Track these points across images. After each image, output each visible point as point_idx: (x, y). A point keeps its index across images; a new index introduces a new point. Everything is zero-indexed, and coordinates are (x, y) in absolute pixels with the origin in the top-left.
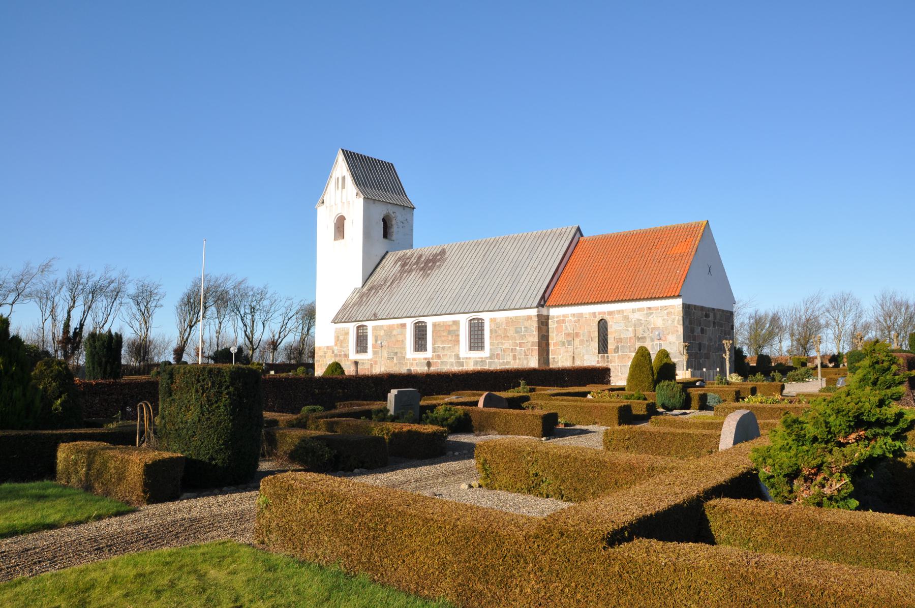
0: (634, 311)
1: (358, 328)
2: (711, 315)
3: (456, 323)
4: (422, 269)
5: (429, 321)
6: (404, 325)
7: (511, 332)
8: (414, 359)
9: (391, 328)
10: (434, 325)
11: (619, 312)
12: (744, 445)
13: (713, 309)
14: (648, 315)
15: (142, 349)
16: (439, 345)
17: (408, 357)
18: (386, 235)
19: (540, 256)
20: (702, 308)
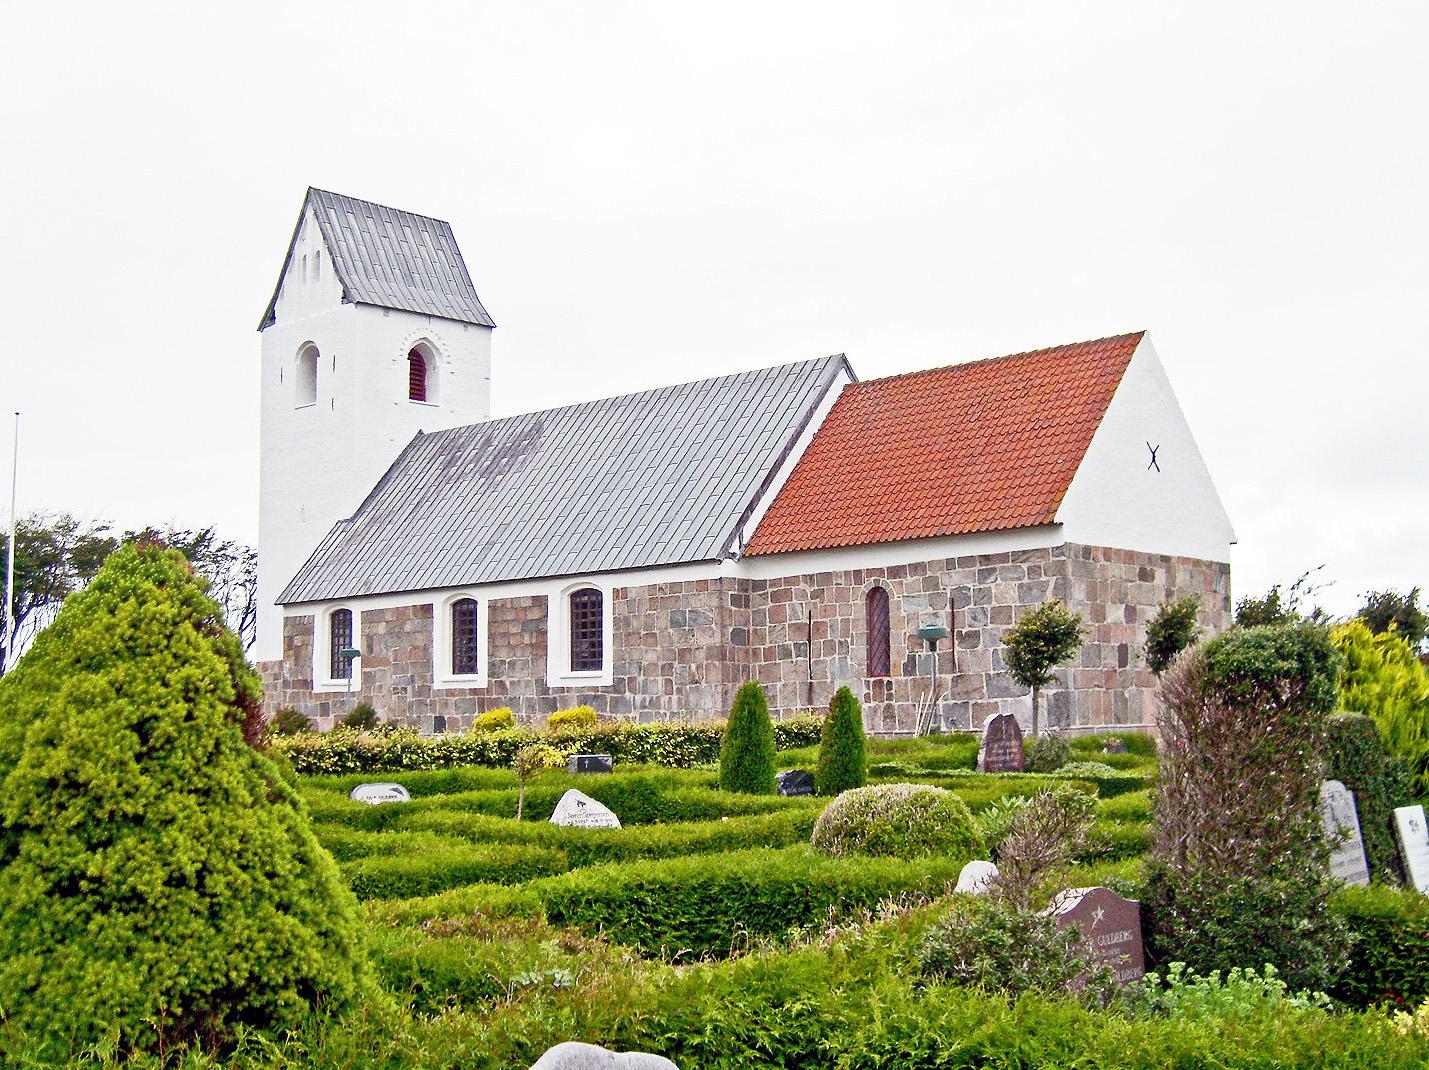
0: (950, 563)
1: (334, 616)
2: (1160, 575)
3: (540, 602)
4: (487, 472)
5: (483, 598)
6: (428, 609)
7: (662, 621)
8: (451, 693)
9: (400, 612)
10: (493, 607)
11: (917, 568)
12: (545, 790)
13: (1166, 559)
14: (984, 575)
15: (1356, 1010)
16: (503, 655)
17: (437, 686)
18: (418, 391)
19: (405, 489)
20: (1130, 556)
